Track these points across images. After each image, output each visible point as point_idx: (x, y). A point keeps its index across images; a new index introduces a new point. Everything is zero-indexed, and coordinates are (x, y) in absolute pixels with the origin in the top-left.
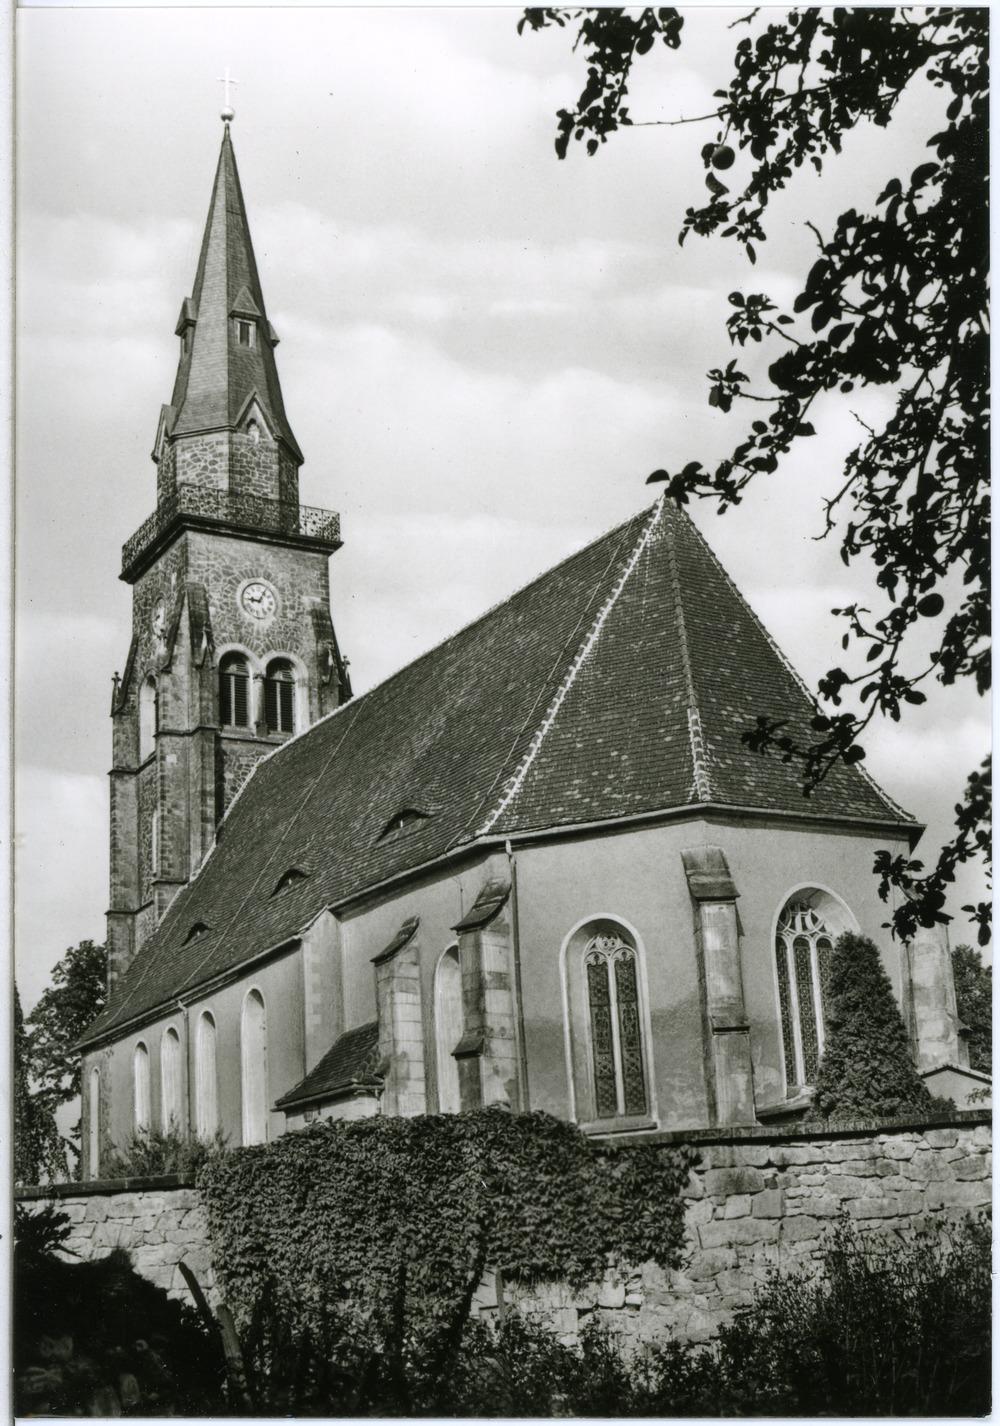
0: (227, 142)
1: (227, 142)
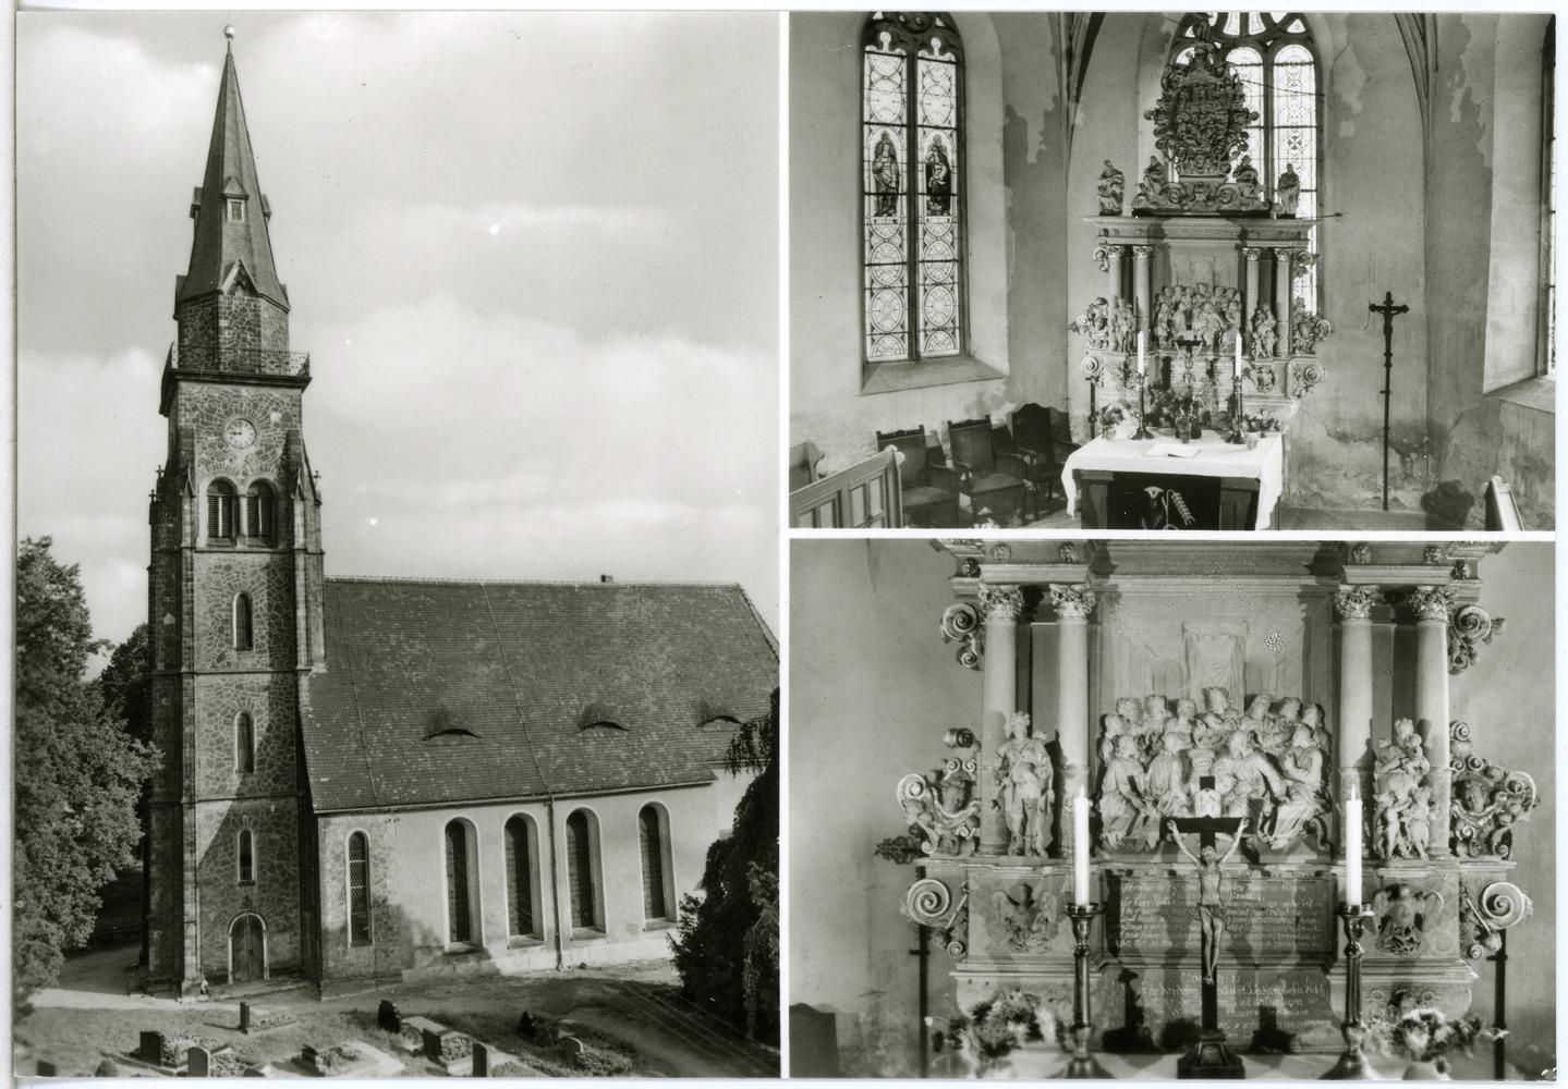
0: (229, 58)
1: (229, 58)
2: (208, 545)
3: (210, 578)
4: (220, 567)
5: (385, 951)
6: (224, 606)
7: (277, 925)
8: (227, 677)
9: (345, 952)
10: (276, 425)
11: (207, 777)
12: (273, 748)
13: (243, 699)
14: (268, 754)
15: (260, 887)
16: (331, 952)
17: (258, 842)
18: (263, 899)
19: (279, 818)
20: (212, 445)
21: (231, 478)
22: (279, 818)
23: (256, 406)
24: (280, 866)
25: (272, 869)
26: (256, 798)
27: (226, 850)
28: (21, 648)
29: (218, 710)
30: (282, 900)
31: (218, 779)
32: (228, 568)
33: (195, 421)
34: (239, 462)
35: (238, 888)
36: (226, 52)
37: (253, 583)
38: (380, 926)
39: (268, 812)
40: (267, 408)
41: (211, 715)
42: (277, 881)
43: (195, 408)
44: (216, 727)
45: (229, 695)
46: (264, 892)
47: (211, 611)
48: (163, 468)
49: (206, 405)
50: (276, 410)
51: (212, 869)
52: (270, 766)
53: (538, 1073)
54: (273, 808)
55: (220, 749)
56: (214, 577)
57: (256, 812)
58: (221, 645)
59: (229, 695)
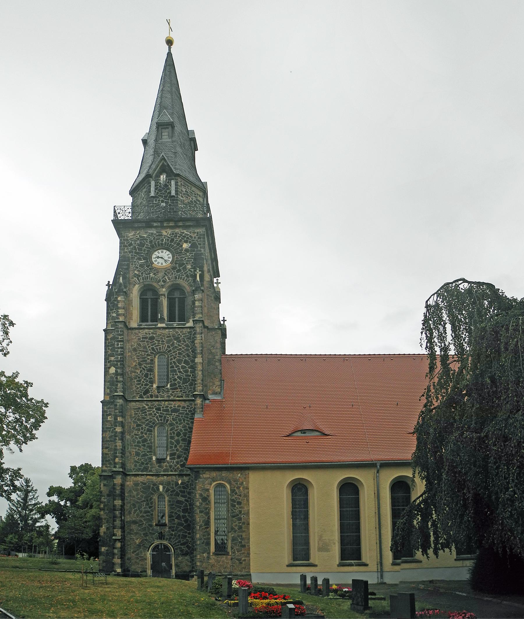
0: (169, 55)
1: (169, 55)
2: (247, 478)
3: (139, 345)
4: (146, 338)
5: (239, 560)
6: (148, 361)
7: (182, 551)
8: (149, 403)
9: (208, 558)
10: (187, 250)
11: (135, 461)
12: (181, 446)
13: (161, 416)
14: (177, 450)
15: (170, 528)
16: (198, 557)
17: (169, 501)
18: (172, 535)
19: (184, 488)
20: (142, 266)
21: (155, 284)
22: (184, 488)
23: (172, 240)
24: (184, 517)
25: (178, 517)
26: (167, 475)
27: (147, 504)
28: (106, 451)
29: (143, 423)
30: (186, 536)
31: (143, 463)
32: (152, 338)
33: (130, 252)
34: (161, 275)
35: (155, 528)
36: (167, 51)
37: (168, 347)
38: (235, 544)
39: (177, 484)
40: (181, 241)
41: (138, 425)
42: (182, 525)
43: (131, 245)
44: (142, 433)
45: (151, 414)
46: (173, 531)
47: (140, 364)
48: (111, 283)
49: (138, 242)
50: (186, 242)
51: (138, 515)
52: (179, 457)
53: (143, 176)
54: (180, 482)
55: (144, 445)
56: (141, 343)
57: (169, 483)
58: (146, 385)
59: (151, 414)
